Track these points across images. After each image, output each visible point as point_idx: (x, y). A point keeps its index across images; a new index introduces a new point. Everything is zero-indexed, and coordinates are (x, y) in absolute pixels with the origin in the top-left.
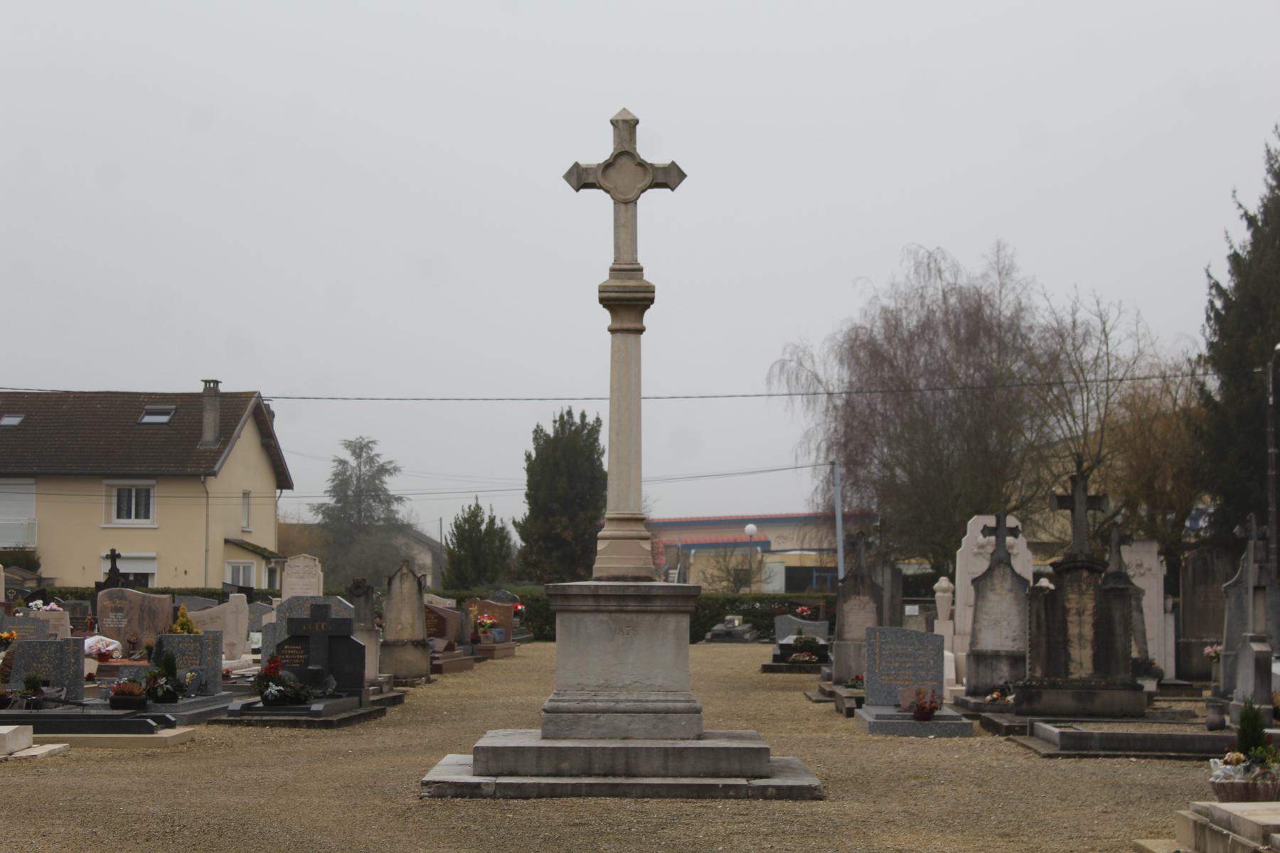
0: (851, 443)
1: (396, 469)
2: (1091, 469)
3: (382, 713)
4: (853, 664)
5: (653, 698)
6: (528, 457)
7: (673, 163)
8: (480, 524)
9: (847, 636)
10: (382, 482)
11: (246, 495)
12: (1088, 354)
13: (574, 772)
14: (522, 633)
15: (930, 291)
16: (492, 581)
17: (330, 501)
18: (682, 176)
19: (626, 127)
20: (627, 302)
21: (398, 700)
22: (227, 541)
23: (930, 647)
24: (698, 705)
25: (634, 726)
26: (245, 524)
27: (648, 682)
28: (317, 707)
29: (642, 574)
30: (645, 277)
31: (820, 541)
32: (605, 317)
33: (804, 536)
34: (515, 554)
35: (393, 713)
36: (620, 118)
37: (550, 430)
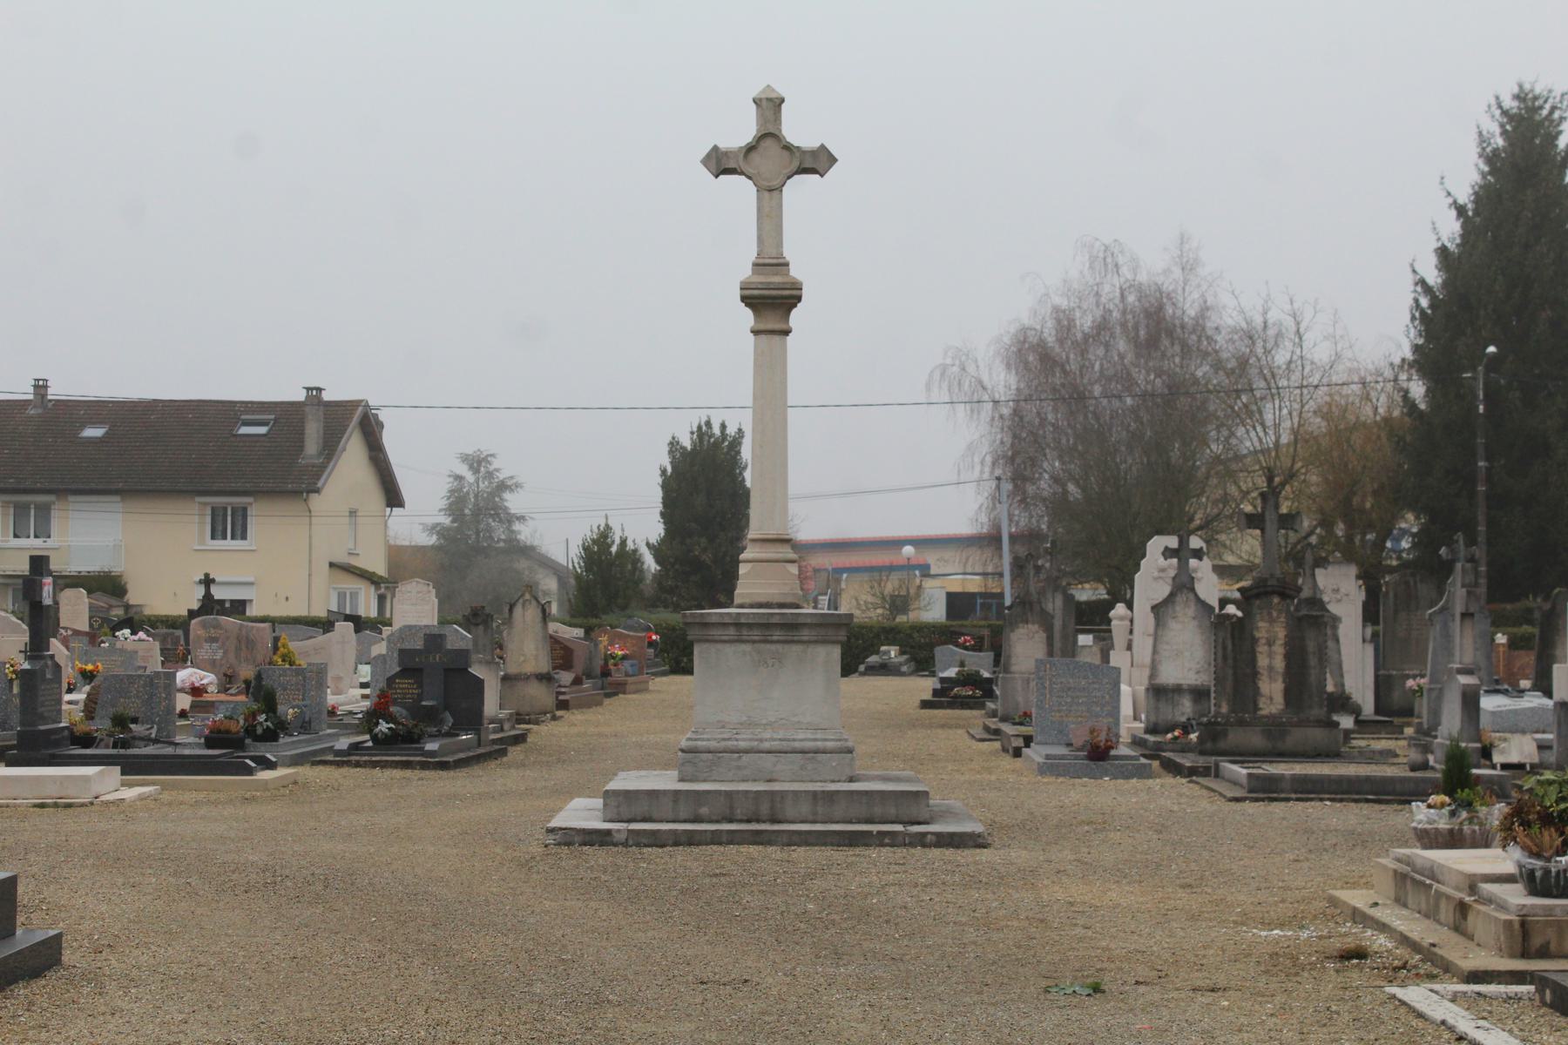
2: (1283, 484)
3: (503, 752)
4: (1020, 699)
5: (801, 736)
6: (664, 472)
7: (823, 147)
9: (1014, 668)
14: (656, 665)
15: (1107, 288)
16: (624, 608)
17: (446, 520)
20: (772, 301)
21: (520, 739)
22: (332, 565)
24: (850, 744)
26: (351, 546)
28: (431, 746)
29: (789, 600)
32: (747, 317)
34: (649, 578)
35: (515, 752)
37: (687, 443)
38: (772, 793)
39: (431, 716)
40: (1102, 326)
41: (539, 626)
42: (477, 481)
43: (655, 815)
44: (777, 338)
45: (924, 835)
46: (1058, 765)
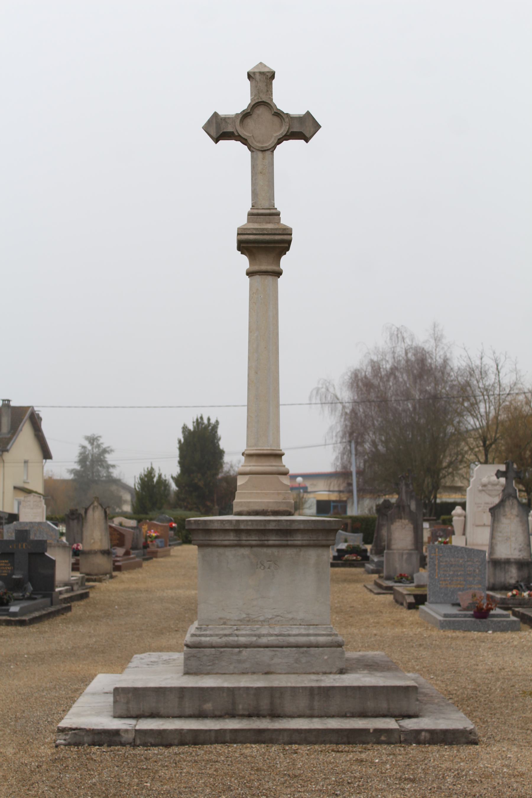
0: (355, 431)
1: (112, 451)
2: (491, 445)
3: (69, 609)
4: (397, 566)
5: (295, 632)
6: (180, 441)
7: (308, 113)
8: (153, 478)
9: (394, 547)
10: (104, 458)
11: (26, 462)
12: (491, 379)
13: (218, 713)
14: (175, 540)
15: (398, 349)
16: (160, 509)
17: (78, 467)
18: (317, 127)
19: (262, 79)
20: (265, 245)
21: (84, 596)
22: (15, 488)
23: (476, 560)
24: (340, 639)
25: (276, 660)
26: (25, 478)
27: (290, 616)
28: (14, 609)
29: (282, 508)
30: (282, 222)
31: (339, 486)
32: (243, 262)
33: (331, 484)
34: (172, 495)
35: (78, 608)
36: (256, 70)
37: (191, 427)
38: (272, 690)
39: (18, 585)
40: (394, 369)
41: (103, 522)
42: (93, 448)
43: (162, 711)
44: (269, 279)
45: (418, 732)
46: (454, 622)
